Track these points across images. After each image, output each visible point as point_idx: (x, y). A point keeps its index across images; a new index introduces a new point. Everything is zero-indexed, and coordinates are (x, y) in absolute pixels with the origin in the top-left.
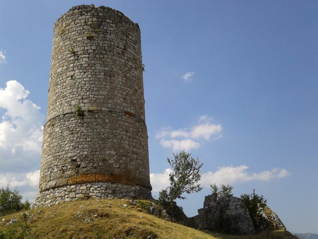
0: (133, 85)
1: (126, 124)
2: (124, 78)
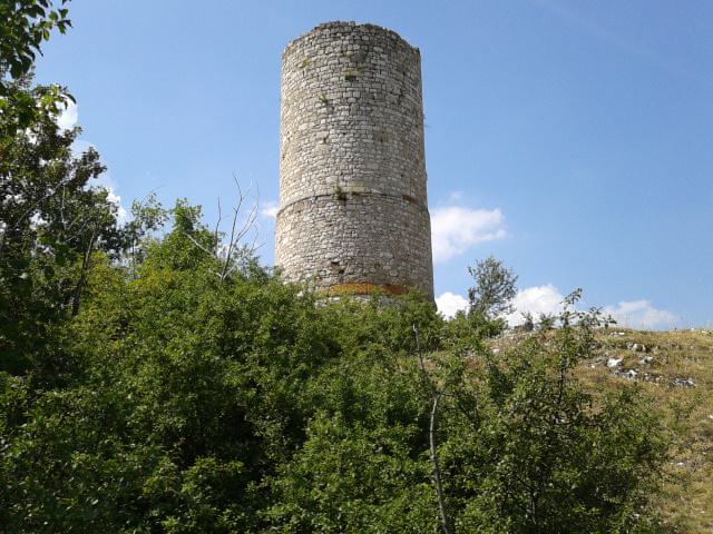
1: (406, 214)
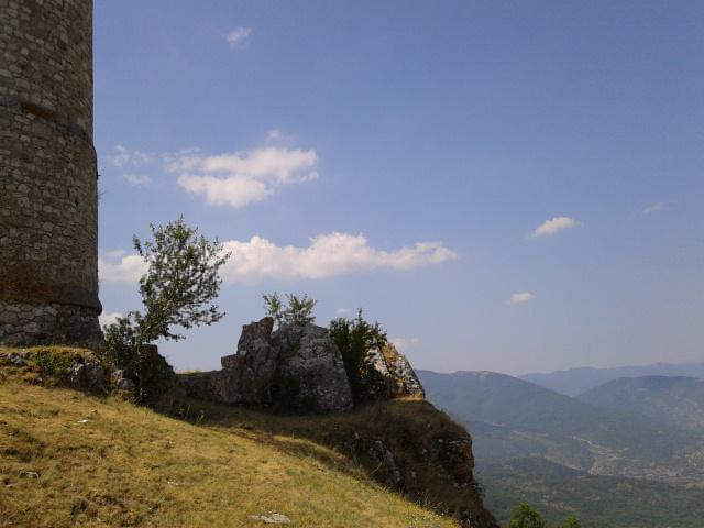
0: (53, 31)
1: (23, 137)
2: (25, 9)
